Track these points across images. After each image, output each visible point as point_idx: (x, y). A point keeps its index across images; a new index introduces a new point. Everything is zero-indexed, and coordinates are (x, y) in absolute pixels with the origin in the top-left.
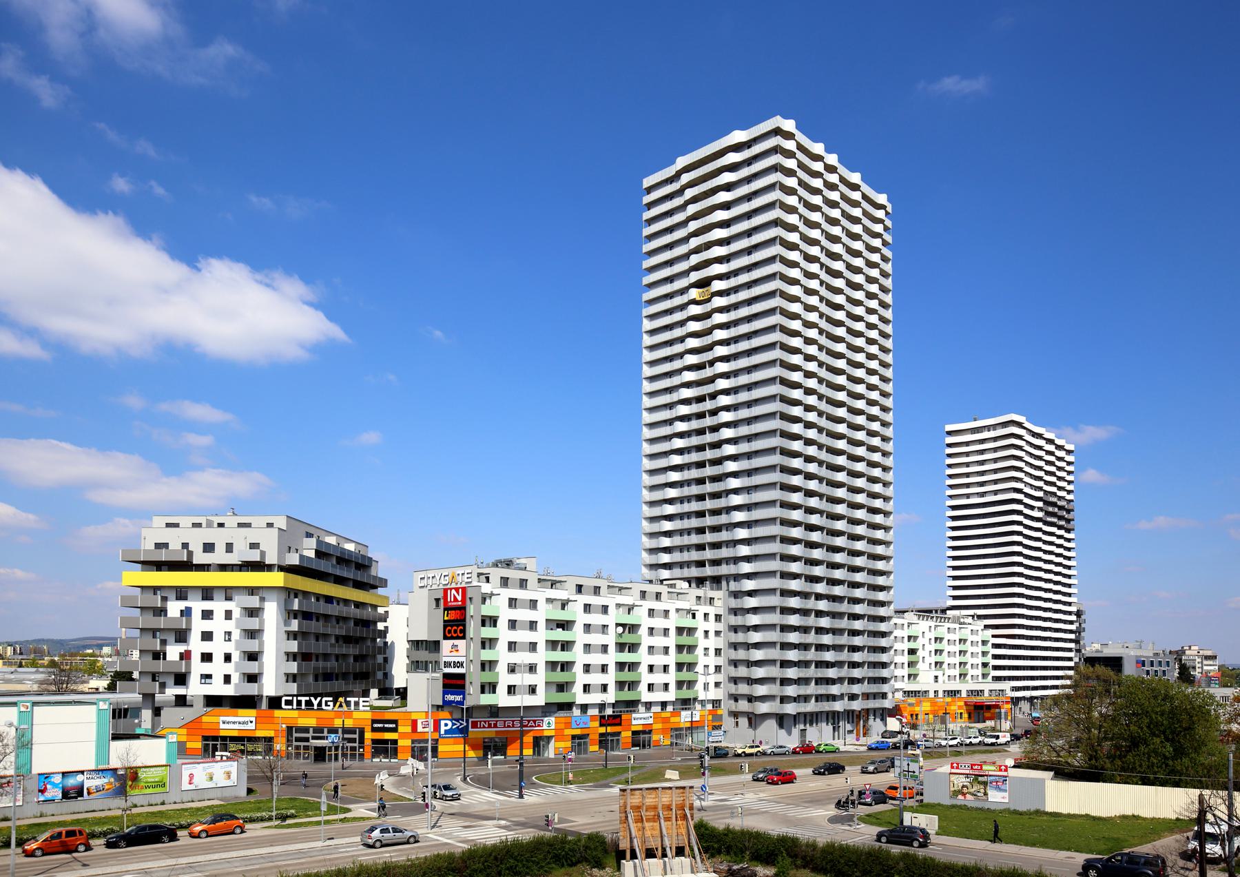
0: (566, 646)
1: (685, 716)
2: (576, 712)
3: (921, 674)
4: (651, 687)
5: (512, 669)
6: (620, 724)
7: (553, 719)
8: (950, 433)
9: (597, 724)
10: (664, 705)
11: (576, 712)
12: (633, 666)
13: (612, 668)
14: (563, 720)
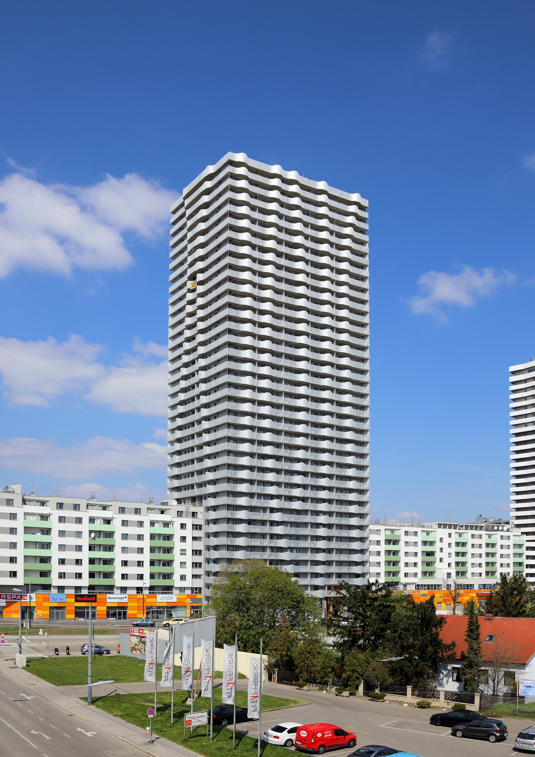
0: (464, 554)
1: (162, 599)
2: (54, 591)
3: (437, 571)
4: (406, 575)
5: (62, 562)
6: (95, 601)
7: (34, 595)
8: (514, 373)
9: (73, 600)
10: (139, 590)
11: (54, 591)
12: (493, 564)
13: (484, 565)
14: (42, 596)
